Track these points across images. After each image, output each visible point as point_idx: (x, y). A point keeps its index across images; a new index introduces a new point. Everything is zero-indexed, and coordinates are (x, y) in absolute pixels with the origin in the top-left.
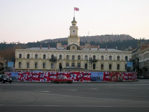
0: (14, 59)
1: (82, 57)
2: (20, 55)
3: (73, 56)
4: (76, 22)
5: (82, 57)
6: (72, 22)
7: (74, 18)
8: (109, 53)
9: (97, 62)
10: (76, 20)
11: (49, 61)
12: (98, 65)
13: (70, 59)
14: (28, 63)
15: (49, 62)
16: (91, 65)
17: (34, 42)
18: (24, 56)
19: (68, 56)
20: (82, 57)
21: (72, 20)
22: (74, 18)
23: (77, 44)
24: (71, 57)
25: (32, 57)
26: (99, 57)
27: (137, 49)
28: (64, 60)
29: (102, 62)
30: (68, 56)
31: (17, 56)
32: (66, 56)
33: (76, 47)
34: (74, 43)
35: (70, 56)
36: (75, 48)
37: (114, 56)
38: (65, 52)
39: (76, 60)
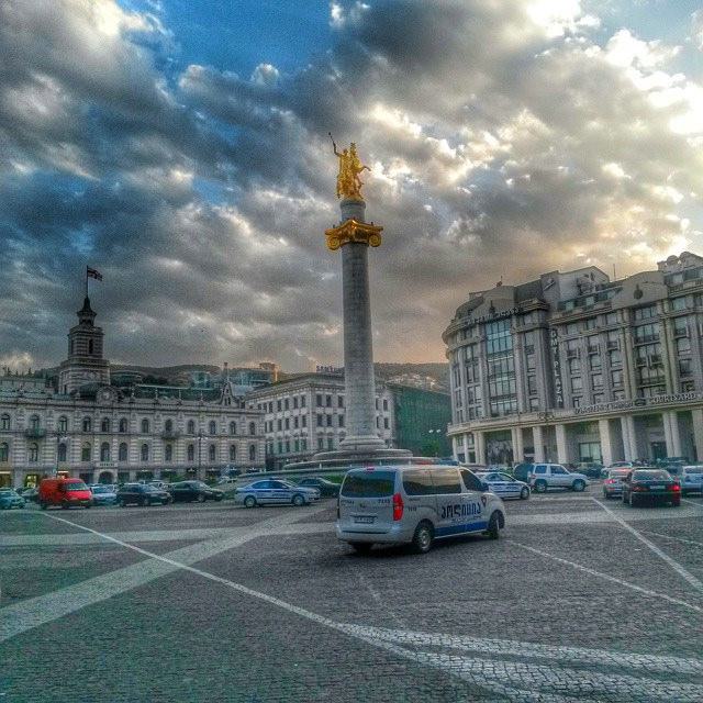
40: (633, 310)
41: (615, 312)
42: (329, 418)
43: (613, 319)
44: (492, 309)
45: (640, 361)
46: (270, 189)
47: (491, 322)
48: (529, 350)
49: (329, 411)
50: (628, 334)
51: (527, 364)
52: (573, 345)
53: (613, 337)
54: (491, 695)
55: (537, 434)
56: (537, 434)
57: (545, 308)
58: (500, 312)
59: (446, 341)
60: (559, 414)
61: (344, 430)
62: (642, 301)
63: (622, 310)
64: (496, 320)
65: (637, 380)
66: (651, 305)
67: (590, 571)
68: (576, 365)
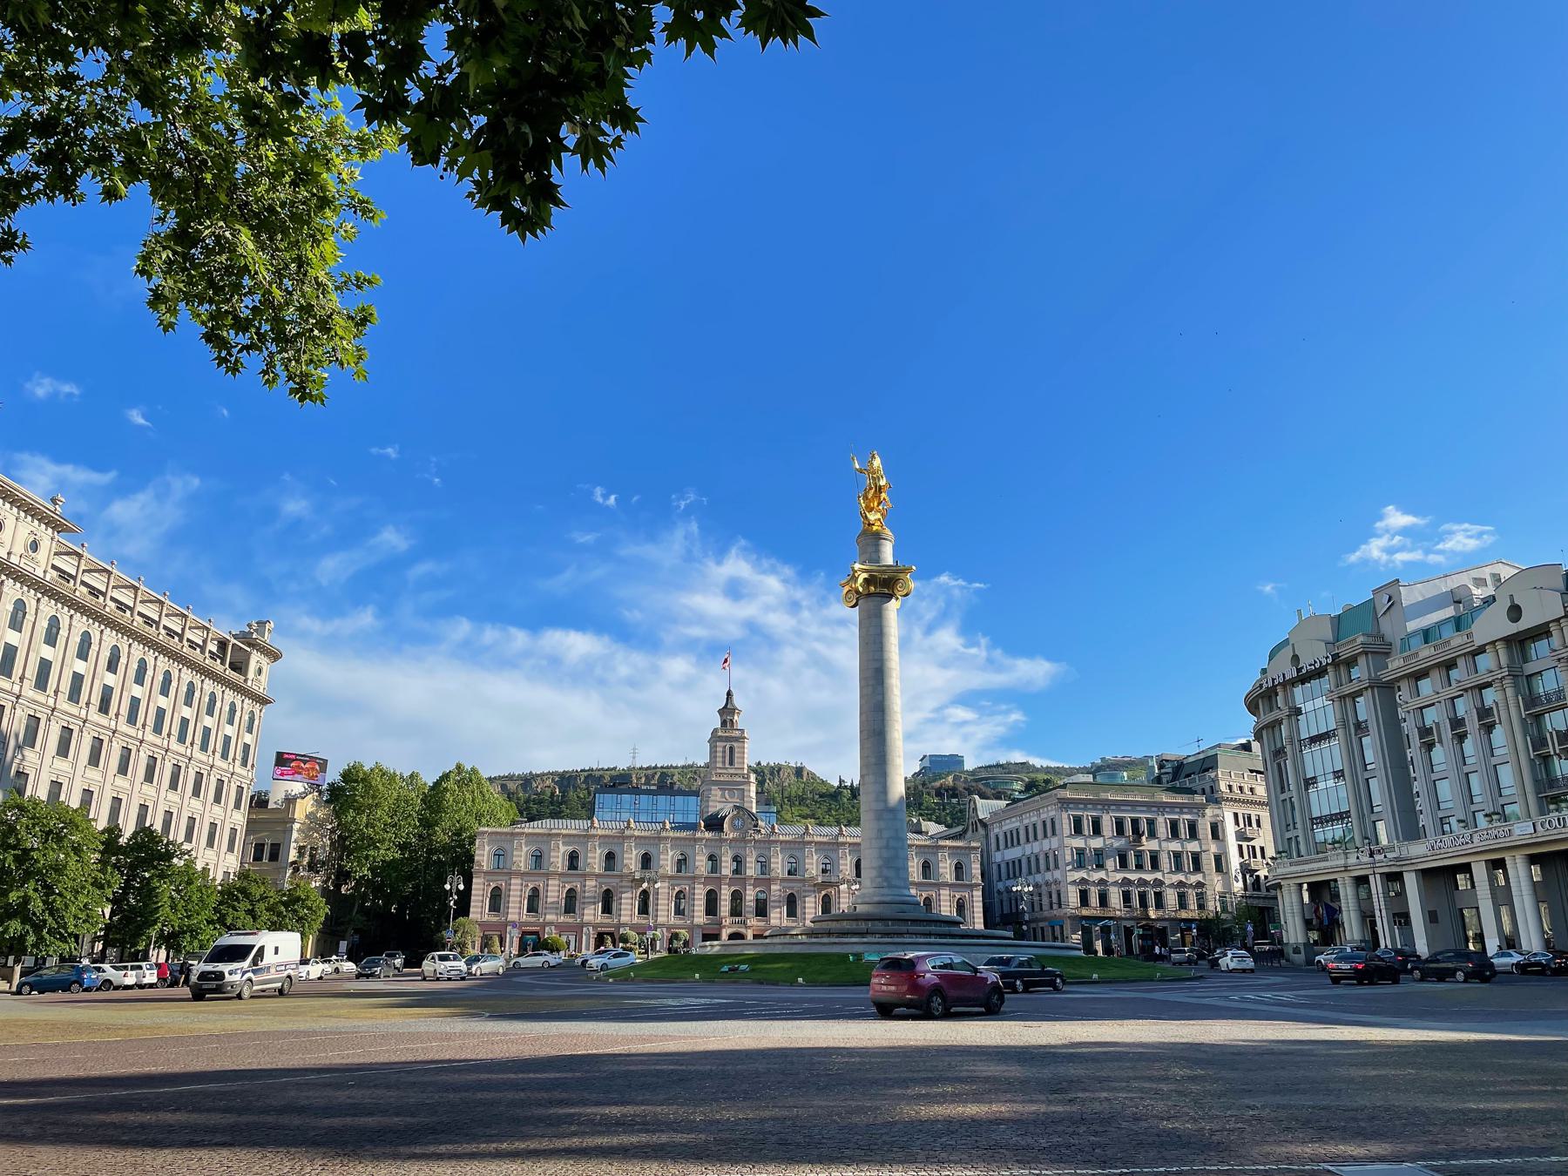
10: (737, 701)
27: (965, 831)
40: (1519, 643)
41: (1481, 650)
42: (1179, 868)
43: (1485, 662)
44: (1295, 659)
45: (1539, 742)
46: (773, 571)
47: (1293, 682)
48: (1361, 728)
49: (1175, 846)
50: (1510, 692)
51: (151, 986)
52: (1431, 716)
53: (1490, 696)
54: (1170, 1145)
55: (1376, 885)
56: (1376, 885)
57: (1380, 650)
58: (1306, 663)
59: (1252, 706)
60: (1417, 849)
61: (1159, 875)
62: (1525, 624)
63: (1493, 643)
64: (1304, 679)
65: (1536, 781)
66: (1542, 632)
67: (1425, 1073)
68: (1438, 754)
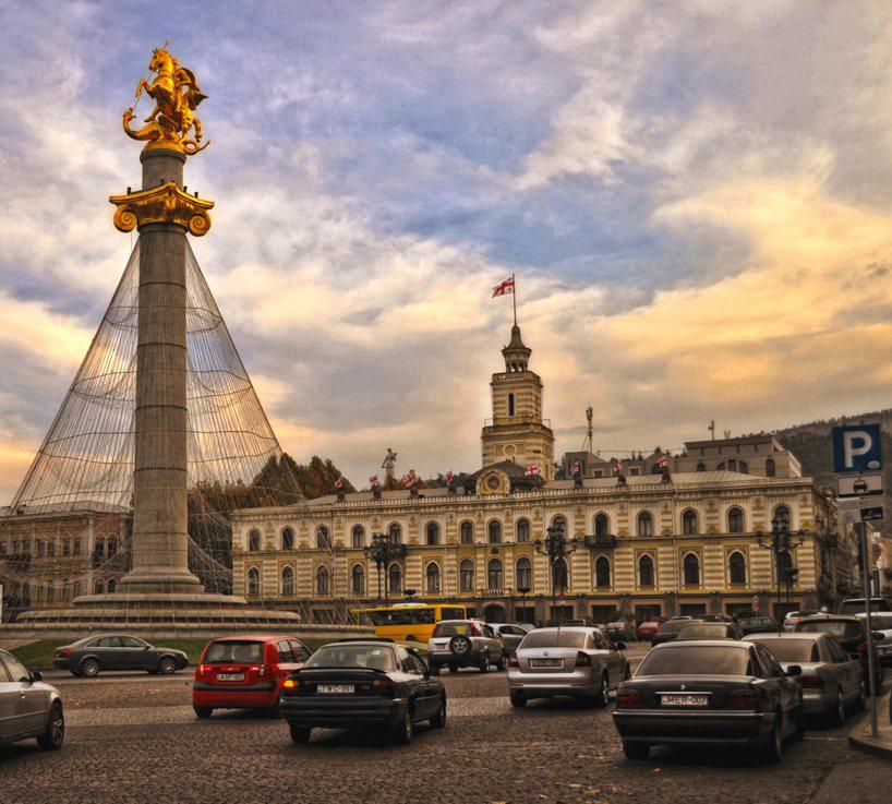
0: (557, 544)
1: (452, 531)
2: (254, 538)
3: (495, 528)
4: (528, 352)
5: (535, 529)
6: (506, 352)
7: (516, 332)
8: (682, 497)
9: (616, 550)
10: (527, 341)
11: (584, 551)
12: (414, 574)
13: (478, 540)
14: (358, 571)
15: (586, 554)
16: (383, 570)
17: (637, 456)
18: (667, 524)
19: (467, 528)
20: (535, 529)
21: (507, 341)
22: (516, 332)
23: (528, 459)
24: (486, 532)
25: (303, 544)
26: (663, 520)
28: (452, 547)
29: (737, 546)
30: (467, 528)
31: (241, 539)
32: (457, 527)
33: (506, 479)
34: (510, 458)
35: (478, 526)
36: (498, 483)
37: (663, 513)
38: (451, 509)
39: (508, 545)
